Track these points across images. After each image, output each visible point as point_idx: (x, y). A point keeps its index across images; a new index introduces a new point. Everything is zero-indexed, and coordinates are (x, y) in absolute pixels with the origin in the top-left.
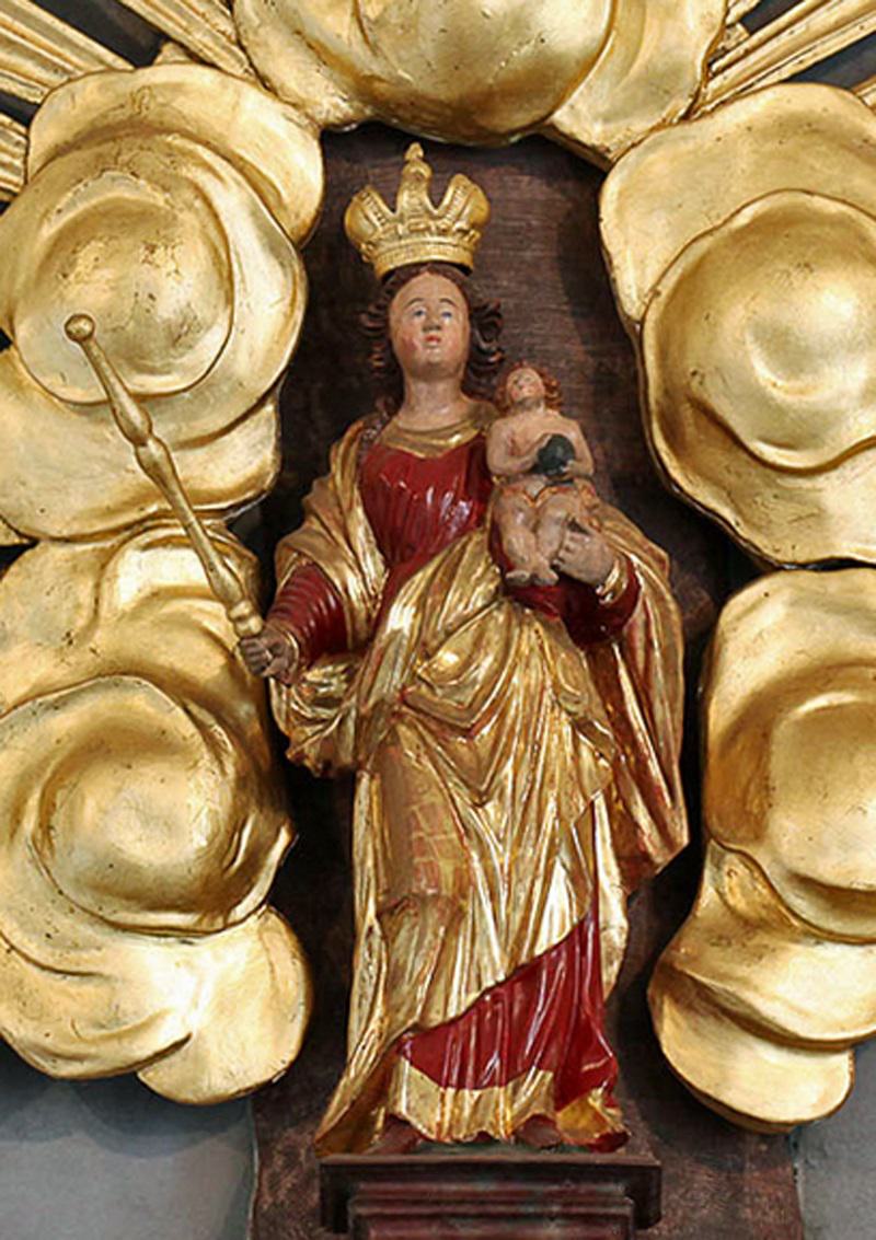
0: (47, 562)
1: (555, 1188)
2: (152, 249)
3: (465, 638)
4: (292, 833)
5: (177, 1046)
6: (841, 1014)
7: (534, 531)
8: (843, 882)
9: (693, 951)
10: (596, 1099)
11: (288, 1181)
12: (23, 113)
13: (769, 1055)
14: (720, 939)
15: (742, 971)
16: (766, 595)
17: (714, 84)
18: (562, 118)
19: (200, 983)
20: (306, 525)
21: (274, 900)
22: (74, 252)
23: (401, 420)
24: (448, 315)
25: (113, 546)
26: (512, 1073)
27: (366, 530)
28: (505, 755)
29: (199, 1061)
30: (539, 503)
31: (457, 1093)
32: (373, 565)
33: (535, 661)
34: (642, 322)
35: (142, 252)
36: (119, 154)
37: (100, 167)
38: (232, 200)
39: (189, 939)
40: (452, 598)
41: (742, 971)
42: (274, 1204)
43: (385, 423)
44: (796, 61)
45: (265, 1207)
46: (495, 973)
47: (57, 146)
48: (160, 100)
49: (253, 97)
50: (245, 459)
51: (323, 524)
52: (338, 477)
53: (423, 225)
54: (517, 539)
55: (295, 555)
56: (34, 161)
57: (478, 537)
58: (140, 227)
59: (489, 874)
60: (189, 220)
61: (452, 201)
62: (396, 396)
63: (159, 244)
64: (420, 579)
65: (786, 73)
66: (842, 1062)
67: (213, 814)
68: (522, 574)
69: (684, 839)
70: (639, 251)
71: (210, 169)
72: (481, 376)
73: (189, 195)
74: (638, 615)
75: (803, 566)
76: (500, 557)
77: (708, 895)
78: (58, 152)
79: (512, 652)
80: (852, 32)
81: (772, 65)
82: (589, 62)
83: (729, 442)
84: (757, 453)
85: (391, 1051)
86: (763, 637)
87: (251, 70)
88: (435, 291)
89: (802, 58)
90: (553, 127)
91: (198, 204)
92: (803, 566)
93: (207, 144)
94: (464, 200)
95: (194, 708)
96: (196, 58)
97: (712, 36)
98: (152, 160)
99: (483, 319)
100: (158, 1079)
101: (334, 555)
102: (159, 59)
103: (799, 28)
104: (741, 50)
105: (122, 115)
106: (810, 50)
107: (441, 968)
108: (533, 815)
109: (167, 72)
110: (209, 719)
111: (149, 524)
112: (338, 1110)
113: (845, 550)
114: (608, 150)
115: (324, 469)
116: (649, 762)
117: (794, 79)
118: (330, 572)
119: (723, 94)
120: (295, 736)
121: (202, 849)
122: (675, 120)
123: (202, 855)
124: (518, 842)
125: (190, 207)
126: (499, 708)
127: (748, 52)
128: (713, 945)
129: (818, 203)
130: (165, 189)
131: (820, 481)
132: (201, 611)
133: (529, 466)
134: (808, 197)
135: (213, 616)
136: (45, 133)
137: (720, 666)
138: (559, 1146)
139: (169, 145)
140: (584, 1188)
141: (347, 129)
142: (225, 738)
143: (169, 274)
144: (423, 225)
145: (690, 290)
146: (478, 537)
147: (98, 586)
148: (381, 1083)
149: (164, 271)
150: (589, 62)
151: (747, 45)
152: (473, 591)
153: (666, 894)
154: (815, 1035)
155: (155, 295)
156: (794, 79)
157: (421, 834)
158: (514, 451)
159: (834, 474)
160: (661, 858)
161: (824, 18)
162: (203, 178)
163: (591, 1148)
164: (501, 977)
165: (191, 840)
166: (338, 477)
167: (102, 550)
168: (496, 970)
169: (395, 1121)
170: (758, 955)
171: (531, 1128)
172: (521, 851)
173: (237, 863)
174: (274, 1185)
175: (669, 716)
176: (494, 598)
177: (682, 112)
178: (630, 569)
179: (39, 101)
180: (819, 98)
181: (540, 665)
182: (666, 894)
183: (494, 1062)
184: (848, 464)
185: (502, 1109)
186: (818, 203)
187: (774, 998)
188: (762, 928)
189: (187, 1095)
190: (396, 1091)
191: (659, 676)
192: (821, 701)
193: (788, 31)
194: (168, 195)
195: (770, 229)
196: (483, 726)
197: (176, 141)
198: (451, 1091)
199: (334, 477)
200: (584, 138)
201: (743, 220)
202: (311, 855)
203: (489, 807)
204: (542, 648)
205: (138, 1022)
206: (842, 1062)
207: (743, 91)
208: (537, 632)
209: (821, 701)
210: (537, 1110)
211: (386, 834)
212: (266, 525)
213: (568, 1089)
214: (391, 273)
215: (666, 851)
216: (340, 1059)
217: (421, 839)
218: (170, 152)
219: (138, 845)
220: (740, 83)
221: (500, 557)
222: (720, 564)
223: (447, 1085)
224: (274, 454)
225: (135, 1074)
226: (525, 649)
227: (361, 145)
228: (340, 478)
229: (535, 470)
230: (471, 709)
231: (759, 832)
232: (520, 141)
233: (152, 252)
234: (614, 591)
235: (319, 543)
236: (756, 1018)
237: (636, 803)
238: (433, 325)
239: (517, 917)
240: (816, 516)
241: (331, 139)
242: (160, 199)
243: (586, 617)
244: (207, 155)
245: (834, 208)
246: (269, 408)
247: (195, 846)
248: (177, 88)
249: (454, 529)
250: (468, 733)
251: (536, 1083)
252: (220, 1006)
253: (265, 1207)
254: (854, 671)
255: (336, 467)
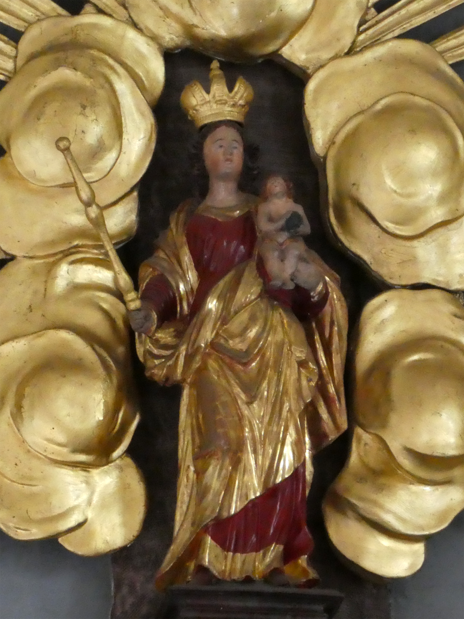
0: (18, 271)
1: (289, 606)
2: (84, 107)
3: (244, 316)
4: (141, 416)
5: (80, 525)
6: (421, 521)
7: (282, 261)
8: (428, 452)
9: (348, 483)
10: (303, 561)
11: (130, 600)
12: (15, 36)
13: (385, 542)
14: (361, 479)
15: (374, 496)
16: (386, 301)
17: (362, 37)
18: (286, 52)
19: (92, 493)
20: (156, 254)
21: (130, 452)
22: (44, 107)
23: (208, 202)
24: (236, 148)
25: (54, 261)
26: (262, 545)
27: (189, 257)
28: (264, 378)
29: (91, 535)
30: (284, 247)
31: (233, 557)
32: (192, 276)
33: (279, 329)
34: (325, 158)
35: (79, 109)
36: (67, 58)
37: (57, 65)
38: (123, 87)
39: (88, 469)
40: (239, 294)
41: (374, 496)
42: (122, 612)
43: (199, 203)
44: (402, 28)
45: (118, 614)
46: (255, 493)
47: (32, 53)
48: (86, 32)
49: (131, 34)
50: (122, 218)
51: (166, 254)
52: (174, 230)
53: (213, 102)
54: (273, 265)
55: (151, 269)
56: (20, 62)
57: (253, 264)
58: (80, 98)
59: (253, 438)
60: (102, 93)
61: (238, 89)
62: (204, 191)
63: (88, 105)
64: (221, 284)
65: (397, 32)
66: (420, 547)
67: (106, 403)
68: (277, 283)
69: (344, 426)
70: (324, 119)
71: (112, 68)
72: (250, 182)
73: (102, 81)
74: (327, 308)
75: (404, 287)
76: (262, 271)
77: (354, 459)
78: (33, 57)
79: (269, 323)
80: (429, 14)
81: (390, 29)
82: (302, 23)
83: (369, 220)
84: (384, 227)
85: (200, 532)
86: (386, 321)
87: (130, 19)
88: (228, 135)
89: (404, 26)
90: (281, 56)
91: (107, 86)
92: (404, 287)
93: (110, 55)
94: (242, 91)
95: (97, 347)
96: (100, 11)
97: (362, 13)
98: (83, 62)
99: (251, 152)
100: (67, 543)
101: (173, 272)
102: (83, 12)
103: (403, 12)
104: (373, 21)
105: (67, 38)
106: (408, 22)
107: (228, 488)
108: (277, 409)
109: (88, 18)
110: (105, 354)
111: (73, 250)
112: (168, 565)
113: (426, 278)
114: (308, 68)
115: (165, 224)
116: (329, 386)
117: (401, 37)
118: (170, 279)
119: (367, 42)
120: (149, 364)
121: (100, 421)
122: (343, 54)
123: (100, 424)
124: (270, 423)
125: (103, 87)
126: (262, 353)
127: (378, 22)
128: (358, 482)
129: (417, 100)
130: (91, 77)
131: (415, 243)
132: (99, 297)
133: (280, 227)
134: (412, 96)
135: (108, 302)
136: (27, 45)
137: (362, 338)
138: (286, 585)
139: (92, 55)
140: (306, 607)
141: (176, 52)
142: (112, 363)
143: (92, 121)
144: (213, 102)
145: (351, 143)
146: (253, 264)
147: (46, 282)
148: (194, 548)
149: (90, 119)
150: (302, 23)
151: (377, 19)
152: (249, 292)
153: (332, 456)
154: (410, 532)
155: (85, 131)
156: (401, 37)
157: (221, 417)
158: (271, 219)
159: (422, 240)
160: (333, 436)
161: (414, 7)
162: (108, 72)
163: (299, 586)
164: (258, 494)
165: (95, 416)
166: (174, 230)
167: (48, 263)
168: (255, 492)
169: (202, 570)
170: (381, 489)
171: (273, 575)
172: (270, 428)
173: (116, 430)
174: (123, 604)
175: (338, 360)
176: (260, 296)
177: (346, 51)
178: (325, 284)
179: (23, 30)
180: (412, 47)
181: (283, 329)
182: (332, 456)
183: (254, 539)
184: (429, 235)
185: (263, 560)
186: (417, 100)
187: (389, 511)
188: (385, 472)
189: (81, 551)
190: (203, 553)
191: (336, 339)
192: (415, 357)
193: (398, 13)
194: (92, 80)
195: (391, 112)
196: (253, 362)
197: (95, 53)
198: (231, 554)
199: (172, 231)
200: (297, 62)
201: (379, 107)
202: (150, 428)
203: (255, 405)
204: (282, 322)
205: (60, 511)
206: (420, 547)
207: (375, 42)
208: (280, 314)
209: (415, 357)
210: (276, 565)
211: (201, 416)
212: (133, 252)
213: (289, 556)
214: (206, 125)
215: (336, 431)
216: (168, 537)
217: (221, 419)
218: (94, 60)
219: (68, 417)
220: (374, 38)
221: (262, 271)
222: (362, 284)
223: (228, 550)
224: (136, 217)
225: (57, 540)
226: (275, 322)
227: (188, 60)
228: (176, 231)
229: (282, 229)
230: (248, 352)
231: (384, 424)
232: (262, 62)
233: (84, 109)
234: (320, 293)
235: (165, 264)
236: (380, 521)
237: (321, 406)
238: (224, 154)
239: (267, 463)
240: (413, 260)
241: (170, 57)
242: (88, 82)
243: (303, 307)
244: (111, 61)
245: (424, 102)
246: (135, 194)
247: (97, 419)
248: (95, 26)
249: (237, 259)
250: (246, 364)
251: (274, 550)
252: (99, 508)
253: (118, 614)
254: (440, 343)
255: (173, 225)
